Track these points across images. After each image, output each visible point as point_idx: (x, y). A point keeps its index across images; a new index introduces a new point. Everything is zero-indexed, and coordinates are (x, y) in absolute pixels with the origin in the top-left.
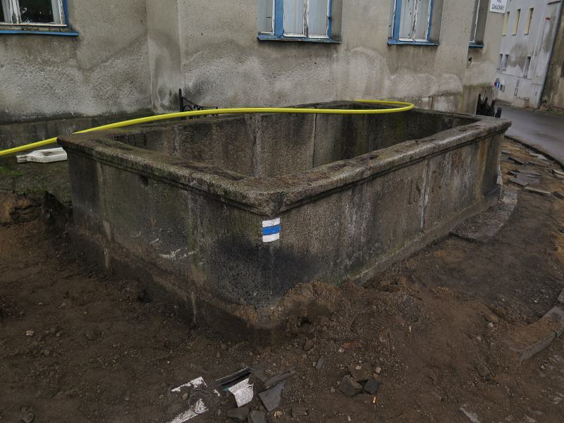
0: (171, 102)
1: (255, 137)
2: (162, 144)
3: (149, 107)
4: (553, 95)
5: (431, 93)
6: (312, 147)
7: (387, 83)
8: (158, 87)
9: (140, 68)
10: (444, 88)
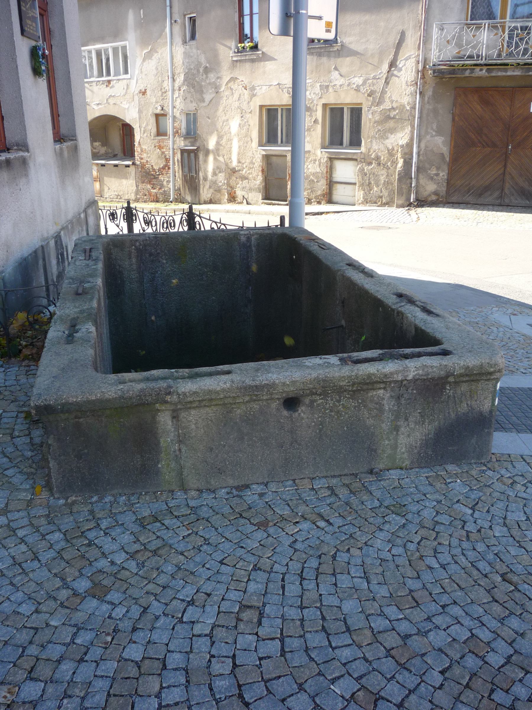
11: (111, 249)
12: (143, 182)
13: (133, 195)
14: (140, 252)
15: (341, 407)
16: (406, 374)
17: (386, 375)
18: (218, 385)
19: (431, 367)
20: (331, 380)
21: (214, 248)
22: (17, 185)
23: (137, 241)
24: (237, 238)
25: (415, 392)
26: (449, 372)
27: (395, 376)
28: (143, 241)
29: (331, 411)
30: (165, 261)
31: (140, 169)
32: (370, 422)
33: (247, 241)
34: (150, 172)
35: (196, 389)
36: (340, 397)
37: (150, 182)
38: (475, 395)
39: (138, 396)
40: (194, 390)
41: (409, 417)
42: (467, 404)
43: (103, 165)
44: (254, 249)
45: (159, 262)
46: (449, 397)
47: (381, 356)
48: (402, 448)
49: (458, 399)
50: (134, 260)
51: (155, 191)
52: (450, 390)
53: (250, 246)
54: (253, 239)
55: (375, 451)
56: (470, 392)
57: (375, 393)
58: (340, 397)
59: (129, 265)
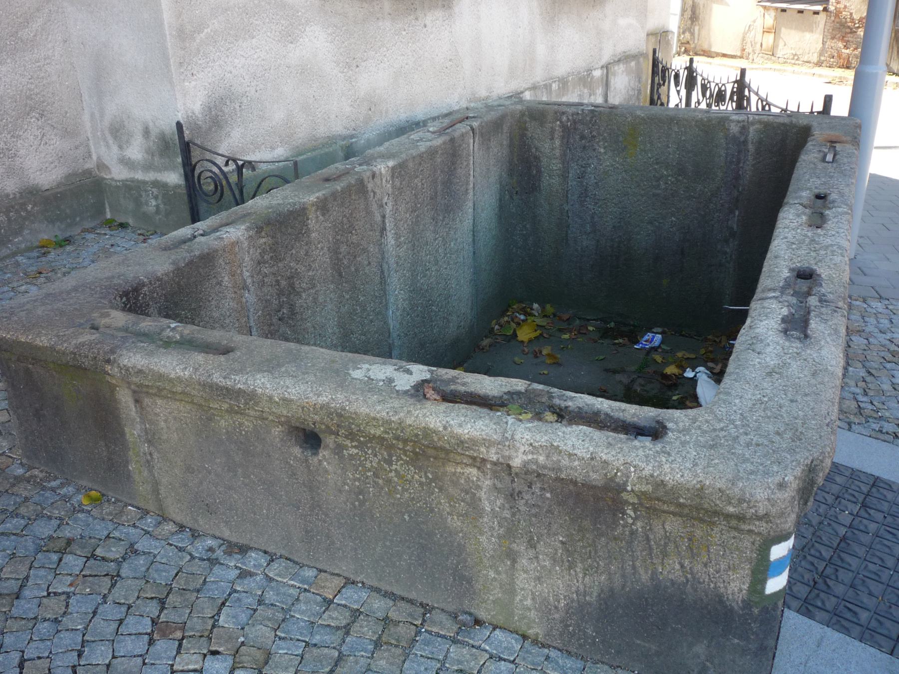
0: (148, 151)
1: (384, 217)
2: (219, 283)
3: (88, 166)
4: (699, 30)
5: (605, 60)
6: (471, 210)
7: (541, 50)
8: (106, 123)
9: (54, 78)
10: (621, 48)
11: (525, 122)
12: (833, 38)
13: (816, 55)
14: (567, 131)
15: (393, 474)
16: (507, 454)
17: (462, 442)
18: (174, 369)
19: (570, 455)
20: (353, 419)
21: (683, 138)
22: (417, 19)
23: (563, 113)
24: (724, 125)
25: (548, 495)
26: (612, 479)
27: (483, 449)
28: (573, 115)
29: (376, 475)
30: (602, 150)
31: (833, 18)
32: (454, 522)
33: (740, 133)
34: (846, 22)
35: (143, 366)
36: (390, 456)
37: (842, 39)
38: (704, 553)
39: (72, 353)
40: (139, 367)
41: (538, 542)
42: (682, 566)
43: (784, 10)
44: (751, 147)
45: (594, 150)
46: (633, 533)
47: (506, 397)
48: (525, 598)
49: (658, 545)
50: (557, 143)
51: (848, 51)
52: (635, 519)
53: (745, 142)
54: (751, 129)
55: (469, 581)
56: (690, 540)
57: (459, 470)
58: (390, 456)
59: (549, 148)
